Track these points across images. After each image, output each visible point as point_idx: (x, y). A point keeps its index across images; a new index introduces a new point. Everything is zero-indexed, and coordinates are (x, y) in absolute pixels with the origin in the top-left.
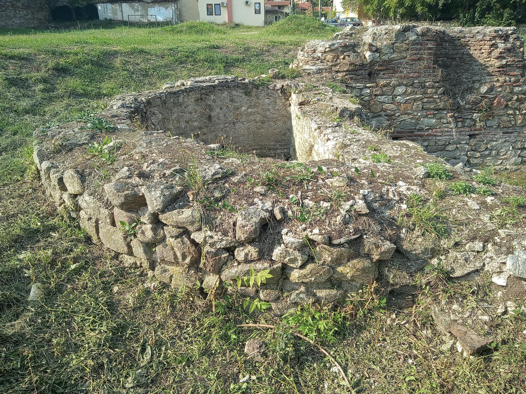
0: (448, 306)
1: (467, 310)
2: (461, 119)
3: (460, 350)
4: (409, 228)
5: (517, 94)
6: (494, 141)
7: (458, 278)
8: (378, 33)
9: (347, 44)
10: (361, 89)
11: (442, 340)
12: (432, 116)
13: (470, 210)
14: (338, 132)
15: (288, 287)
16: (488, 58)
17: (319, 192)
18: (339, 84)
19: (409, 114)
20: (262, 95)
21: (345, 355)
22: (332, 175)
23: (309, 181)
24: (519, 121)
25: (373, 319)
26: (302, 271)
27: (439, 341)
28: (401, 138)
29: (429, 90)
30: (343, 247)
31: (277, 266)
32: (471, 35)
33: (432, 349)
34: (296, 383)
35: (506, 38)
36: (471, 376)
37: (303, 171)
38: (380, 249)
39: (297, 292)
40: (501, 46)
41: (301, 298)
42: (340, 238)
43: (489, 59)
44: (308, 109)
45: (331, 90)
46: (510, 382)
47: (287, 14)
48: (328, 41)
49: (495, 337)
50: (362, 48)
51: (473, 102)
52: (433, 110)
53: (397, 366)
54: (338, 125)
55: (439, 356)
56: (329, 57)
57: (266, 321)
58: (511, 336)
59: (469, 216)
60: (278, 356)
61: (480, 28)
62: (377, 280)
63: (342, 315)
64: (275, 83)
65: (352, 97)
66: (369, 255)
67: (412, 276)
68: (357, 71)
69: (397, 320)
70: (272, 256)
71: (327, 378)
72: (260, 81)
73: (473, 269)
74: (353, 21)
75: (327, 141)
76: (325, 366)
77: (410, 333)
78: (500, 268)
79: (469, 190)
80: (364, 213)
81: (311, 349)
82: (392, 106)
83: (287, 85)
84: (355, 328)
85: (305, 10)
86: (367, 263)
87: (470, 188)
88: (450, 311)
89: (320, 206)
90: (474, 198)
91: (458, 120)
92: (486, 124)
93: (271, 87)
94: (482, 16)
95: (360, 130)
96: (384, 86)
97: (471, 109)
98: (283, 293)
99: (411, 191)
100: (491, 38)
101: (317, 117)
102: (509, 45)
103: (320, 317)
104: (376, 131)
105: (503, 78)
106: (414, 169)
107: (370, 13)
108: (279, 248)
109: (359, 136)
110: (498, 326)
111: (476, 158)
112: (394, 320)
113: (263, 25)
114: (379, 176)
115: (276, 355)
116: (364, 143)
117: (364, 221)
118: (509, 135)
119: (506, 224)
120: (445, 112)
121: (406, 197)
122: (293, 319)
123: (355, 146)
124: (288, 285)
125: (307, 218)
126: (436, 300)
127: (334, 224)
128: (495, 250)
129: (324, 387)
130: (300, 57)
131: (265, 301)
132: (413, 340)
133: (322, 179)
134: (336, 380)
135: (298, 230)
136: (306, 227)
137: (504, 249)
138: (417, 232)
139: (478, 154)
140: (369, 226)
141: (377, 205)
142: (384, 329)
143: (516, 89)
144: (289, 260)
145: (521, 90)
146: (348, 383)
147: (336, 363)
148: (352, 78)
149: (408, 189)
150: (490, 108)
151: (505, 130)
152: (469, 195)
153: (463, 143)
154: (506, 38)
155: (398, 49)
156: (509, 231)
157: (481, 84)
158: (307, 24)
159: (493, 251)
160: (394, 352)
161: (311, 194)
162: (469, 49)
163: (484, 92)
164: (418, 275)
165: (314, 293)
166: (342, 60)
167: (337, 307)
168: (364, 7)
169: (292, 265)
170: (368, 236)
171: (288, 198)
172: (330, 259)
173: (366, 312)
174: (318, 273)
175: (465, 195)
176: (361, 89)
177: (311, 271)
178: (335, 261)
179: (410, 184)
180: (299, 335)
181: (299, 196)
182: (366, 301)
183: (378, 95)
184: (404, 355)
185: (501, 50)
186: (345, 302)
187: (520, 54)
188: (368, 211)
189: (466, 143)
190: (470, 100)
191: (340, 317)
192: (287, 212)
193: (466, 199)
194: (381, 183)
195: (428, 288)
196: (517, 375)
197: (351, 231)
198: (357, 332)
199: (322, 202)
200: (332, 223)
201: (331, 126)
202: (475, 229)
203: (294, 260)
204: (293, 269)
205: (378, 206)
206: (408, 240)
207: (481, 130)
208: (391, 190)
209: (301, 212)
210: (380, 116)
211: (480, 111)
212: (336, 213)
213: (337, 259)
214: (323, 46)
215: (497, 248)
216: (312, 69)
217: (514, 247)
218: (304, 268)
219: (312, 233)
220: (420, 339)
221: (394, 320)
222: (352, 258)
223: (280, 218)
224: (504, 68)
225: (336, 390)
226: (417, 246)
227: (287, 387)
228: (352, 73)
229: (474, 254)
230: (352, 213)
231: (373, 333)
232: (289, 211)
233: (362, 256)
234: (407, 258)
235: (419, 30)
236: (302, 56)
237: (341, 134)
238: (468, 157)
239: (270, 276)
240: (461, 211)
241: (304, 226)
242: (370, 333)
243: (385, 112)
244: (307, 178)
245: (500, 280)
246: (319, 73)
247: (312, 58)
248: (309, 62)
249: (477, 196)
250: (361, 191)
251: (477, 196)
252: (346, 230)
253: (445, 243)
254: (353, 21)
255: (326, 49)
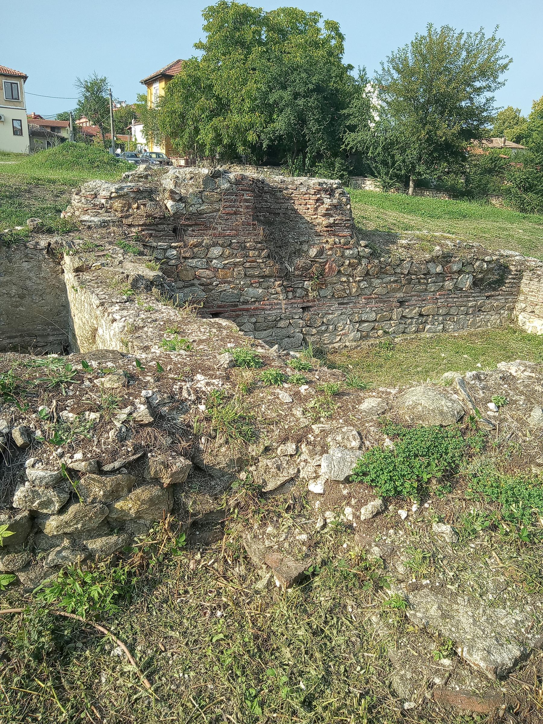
0: (261, 531)
1: (283, 531)
2: (291, 289)
3: (278, 584)
4: (210, 435)
5: (349, 258)
6: (329, 314)
7: (271, 492)
8: (180, 176)
9: (141, 188)
10: (165, 250)
11: (258, 575)
12: (258, 285)
13: (282, 404)
14: (128, 310)
15: (43, 544)
16: (315, 215)
17: (84, 398)
18: (132, 243)
19: (229, 283)
20: (18, 257)
21: (132, 626)
22: (103, 372)
23: (69, 384)
24: (354, 290)
25: (171, 566)
26: (62, 517)
27: (253, 578)
28: (222, 313)
29: (251, 252)
30: (119, 473)
31: (20, 516)
32: (294, 187)
33: (246, 590)
34: (56, 688)
35: (331, 192)
36: (289, 616)
37: (61, 369)
38: (170, 469)
39: (58, 549)
40: (327, 201)
41: (64, 558)
42: (113, 462)
43: (316, 216)
44: (87, 277)
45: (122, 251)
46: (331, 611)
47: (63, 140)
48: (113, 183)
49: (315, 559)
50: (161, 196)
51: (302, 267)
52: (258, 277)
53: (202, 625)
54: (129, 300)
55: (253, 598)
56: (117, 204)
57: (11, 603)
58: (331, 554)
59: (280, 411)
60: (26, 655)
61: (303, 179)
62: (172, 512)
63: (126, 570)
64: (37, 240)
65: (150, 261)
66: (157, 479)
67: (216, 499)
68: (157, 225)
69: (202, 561)
70: (12, 503)
71: (106, 668)
72: (11, 235)
73: (287, 478)
74: (159, 157)
75: (112, 323)
76: (103, 650)
77: (219, 576)
78: (315, 472)
79: (280, 379)
80: (147, 422)
81: (82, 630)
82: (208, 272)
83: (56, 242)
84: (147, 585)
85: (91, 136)
86: (155, 491)
87: (281, 377)
88: (264, 536)
89: (85, 419)
90: (286, 389)
91: (288, 289)
92: (319, 294)
93: (31, 245)
94: (313, 164)
95: (160, 306)
96: (195, 246)
97: (301, 276)
98: (35, 555)
99: (212, 387)
100: (315, 192)
101: (100, 289)
102: (335, 201)
103: (94, 580)
104: (180, 306)
105: (332, 239)
106: (218, 357)
107: (180, 148)
108: (22, 488)
109: (157, 314)
110: (317, 543)
111: (312, 335)
112: (198, 562)
113: (27, 152)
114: (171, 369)
115: (24, 653)
116: (162, 323)
117: (148, 434)
118: (345, 306)
119: (320, 418)
120: (273, 280)
121: (205, 395)
122: (52, 592)
123: (151, 329)
124: (44, 541)
125: (64, 438)
126: (248, 525)
127: (105, 443)
128: (310, 452)
129: (100, 681)
130: (74, 203)
131: (7, 572)
132: (222, 583)
133: (89, 379)
134: (118, 667)
135: (51, 458)
136: (63, 452)
137: (318, 448)
138: (220, 440)
139: (314, 330)
140: (155, 439)
141: (166, 409)
142: (186, 577)
143: (347, 252)
144: (39, 504)
145: (353, 254)
146: (135, 666)
147: (119, 642)
148: (151, 235)
149: (208, 384)
150: (321, 275)
151: (341, 300)
152: (281, 386)
153: (296, 317)
154: (331, 192)
155: (207, 199)
156: (323, 426)
157: (310, 246)
158: (91, 156)
159: (307, 452)
160: (198, 606)
161: (72, 403)
162: (294, 203)
163: (314, 255)
164: (224, 497)
165: (85, 546)
166: (135, 210)
167: (118, 558)
168: (172, 141)
169: (45, 511)
170: (154, 454)
171: (35, 412)
172: (102, 493)
173: (161, 558)
174: (86, 516)
175: (276, 386)
176: (165, 250)
177: (75, 514)
178: (110, 495)
179: (211, 376)
180: (62, 613)
181: (53, 406)
182: (160, 543)
183: (188, 258)
184: (211, 606)
185: (327, 206)
186: (130, 550)
187: (348, 212)
188: (152, 419)
189: (300, 318)
190: (299, 265)
191: (124, 574)
192: (34, 432)
193: (278, 391)
194: (172, 379)
195: (236, 511)
196: (338, 601)
197: (129, 449)
198: (150, 590)
199: (87, 413)
200: (103, 441)
201: (118, 301)
202: (286, 427)
203: (48, 503)
204: (47, 516)
205: (167, 411)
206: (209, 451)
207: (315, 301)
208: (185, 387)
209: (57, 431)
210: (193, 285)
211: (311, 278)
212: (109, 427)
213: (113, 492)
214: (107, 189)
215: (311, 447)
216: (93, 221)
217: (329, 445)
218: (66, 512)
219: (73, 460)
220: (231, 581)
221: (198, 562)
222: (135, 486)
223: (22, 443)
224: (332, 227)
225: (118, 682)
226: (220, 458)
227: (42, 699)
228: (151, 228)
229: (287, 458)
230: (131, 423)
231: (171, 586)
232: (36, 432)
233: (148, 483)
234: (210, 475)
235: (232, 176)
236: (78, 202)
237: (132, 312)
238: (303, 334)
239: (10, 533)
240: (271, 407)
241: (60, 450)
242: (167, 587)
243: (199, 280)
244: (66, 380)
245: (316, 488)
246: (104, 227)
247: (92, 205)
248: (89, 211)
249: (290, 386)
250: (144, 393)
251: (290, 386)
252: (123, 449)
253: (254, 450)
254: (159, 157)
255: (112, 193)
